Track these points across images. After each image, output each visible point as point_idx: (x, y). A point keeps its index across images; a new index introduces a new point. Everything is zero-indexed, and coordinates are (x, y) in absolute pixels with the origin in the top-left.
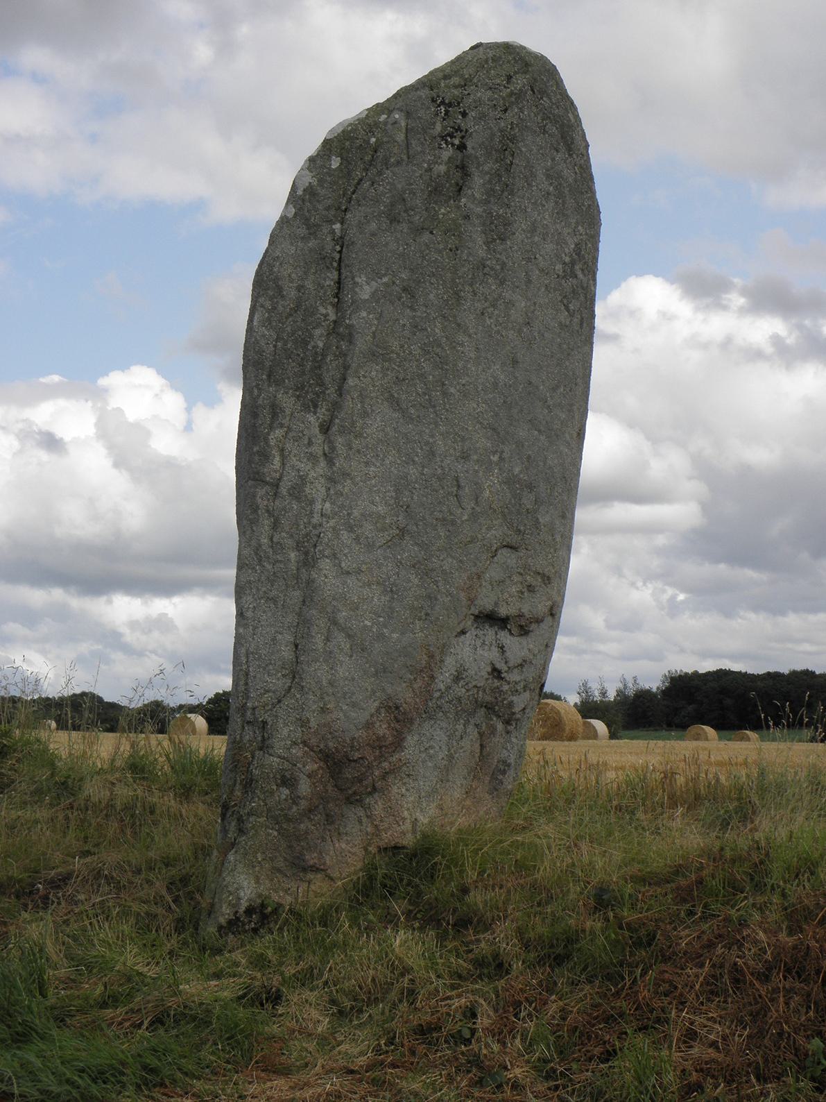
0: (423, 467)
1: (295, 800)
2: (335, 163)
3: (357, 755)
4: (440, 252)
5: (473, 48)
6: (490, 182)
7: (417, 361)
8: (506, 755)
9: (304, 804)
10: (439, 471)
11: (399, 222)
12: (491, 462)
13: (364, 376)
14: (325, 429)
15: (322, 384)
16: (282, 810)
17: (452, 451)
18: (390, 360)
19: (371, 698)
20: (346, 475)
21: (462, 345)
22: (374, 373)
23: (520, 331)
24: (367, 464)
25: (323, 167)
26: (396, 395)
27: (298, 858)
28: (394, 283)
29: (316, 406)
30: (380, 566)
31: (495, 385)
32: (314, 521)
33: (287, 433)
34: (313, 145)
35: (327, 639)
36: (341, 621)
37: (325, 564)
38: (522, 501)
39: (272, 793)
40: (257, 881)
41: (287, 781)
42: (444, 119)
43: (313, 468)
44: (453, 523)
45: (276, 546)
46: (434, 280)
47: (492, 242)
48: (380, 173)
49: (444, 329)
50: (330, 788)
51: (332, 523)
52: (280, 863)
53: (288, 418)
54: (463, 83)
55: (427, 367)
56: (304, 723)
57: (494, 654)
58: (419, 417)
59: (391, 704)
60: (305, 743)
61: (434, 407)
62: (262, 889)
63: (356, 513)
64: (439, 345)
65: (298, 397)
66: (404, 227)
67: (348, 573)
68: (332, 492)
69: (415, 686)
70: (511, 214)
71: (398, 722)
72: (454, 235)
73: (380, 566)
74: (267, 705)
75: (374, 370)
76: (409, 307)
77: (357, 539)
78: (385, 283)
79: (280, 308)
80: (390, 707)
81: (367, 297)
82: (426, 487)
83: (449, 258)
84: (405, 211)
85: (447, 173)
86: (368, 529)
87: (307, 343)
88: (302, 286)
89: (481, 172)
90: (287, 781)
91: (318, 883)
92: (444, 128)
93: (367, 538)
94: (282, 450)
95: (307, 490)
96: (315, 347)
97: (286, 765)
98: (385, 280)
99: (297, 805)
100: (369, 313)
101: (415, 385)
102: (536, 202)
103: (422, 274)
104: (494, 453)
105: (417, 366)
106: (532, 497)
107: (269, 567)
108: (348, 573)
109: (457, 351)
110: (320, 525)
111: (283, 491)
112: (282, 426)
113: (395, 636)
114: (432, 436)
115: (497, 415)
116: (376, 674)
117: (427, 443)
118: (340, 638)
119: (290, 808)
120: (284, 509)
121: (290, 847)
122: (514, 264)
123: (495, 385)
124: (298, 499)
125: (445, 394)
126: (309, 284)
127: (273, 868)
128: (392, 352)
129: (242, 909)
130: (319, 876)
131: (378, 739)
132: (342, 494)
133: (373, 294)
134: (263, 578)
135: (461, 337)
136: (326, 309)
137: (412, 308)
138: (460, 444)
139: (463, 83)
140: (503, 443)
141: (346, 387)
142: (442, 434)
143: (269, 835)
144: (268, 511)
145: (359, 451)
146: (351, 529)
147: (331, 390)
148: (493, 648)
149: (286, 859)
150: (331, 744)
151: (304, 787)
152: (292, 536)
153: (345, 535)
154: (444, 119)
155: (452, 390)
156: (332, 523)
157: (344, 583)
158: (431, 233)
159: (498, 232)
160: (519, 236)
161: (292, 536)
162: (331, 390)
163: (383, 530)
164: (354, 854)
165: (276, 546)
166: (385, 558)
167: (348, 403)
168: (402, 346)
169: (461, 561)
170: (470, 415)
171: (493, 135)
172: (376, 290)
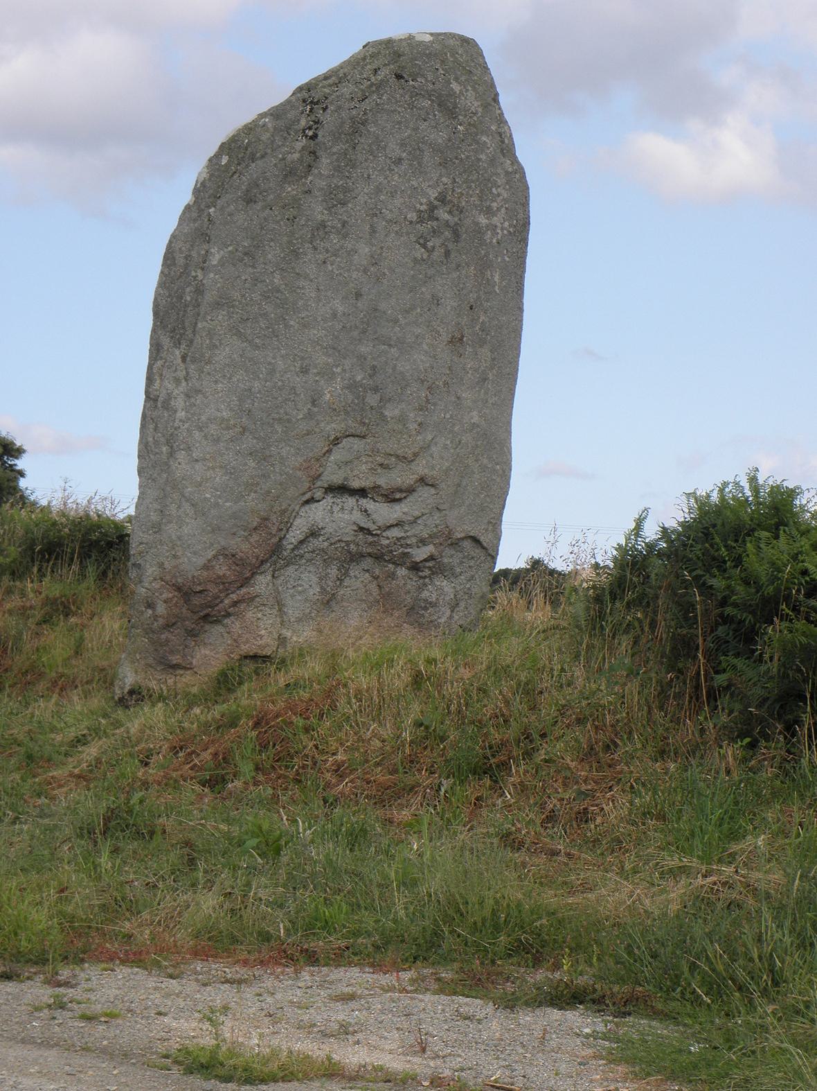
0: (266, 382)
1: (155, 618)
2: (225, 160)
3: (199, 588)
4: (278, 222)
5: (364, 47)
6: (337, 160)
7: (259, 304)
8: (428, 594)
9: (161, 621)
10: (280, 383)
11: (255, 202)
12: (334, 373)
13: (212, 320)
14: (184, 358)
15: (184, 328)
16: (148, 624)
17: (292, 368)
18: (233, 306)
19: (209, 548)
20: (198, 391)
21: (303, 288)
22: (220, 317)
23: (365, 271)
24: (216, 382)
25: (217, 164)
26: (243, 331)
27: (163, 658)
28: (237, 250)
29: (180, 344)
30: (222, 455)
31: (334, 315)
32: (176, 425)
33: (165, 363)
34: (212, 150)
35: (179, 507)
36: (187, 495)
37: (181, 456)
38: (366, 400)
39: (142, 612)
40: (136, 672)
41: (150, 605)
42: (309, 115)
43: (177, 387)
44: (289, 421)
45: (156, 443)
46: (272, 244)
47: (333, 207)
48: (247, 166)
49: (283, 278)
50: (184, 610)
51: (186, 425)
52: (151, 661)
53: (165, 353)
54: (337, 82)
55: (269, 308)
56: (161, 565)
57: (357, 516)
58: (264, 344)
59: (227, 553)
60: (162, 579)
61: (277, 336)
62: (139, 678)
63: (203, 418)
64: (278, 291)
65: (172, 337)
66: (259, 206)
67: (197, 461)
68: (187, 404)
69: (252, 540)
70: (353, 183)
71: (237, 565)
72: (293, 208)
73: (222, 455)
74: (143, 552)
75: (221, 315)
76: (250, 266)
77: (205, 437)
78: (230, 251)
79: (172, 273)
80: (226, 555)
81: (215, 263)
82: (268, 396)
83: (286, 225)
84: (260, 194)
85: (301, 160)
86: (213, 429)
87: (182, 299)
88: (190, 256)
89: (328, 154)
90: (150, 605)
91: (186, 678)
92: (308, 122)
93: (212, 435)
94: (161, 375)
95: (173, 403)
96: (185, 301)
97: (150, 594)
98: (230, 248)
99: (157, 621)
100: (215, 275)
101: (258, 322)
102: (383, 168)
103: (261, 241)
104: (337, 366)
105: (259, 308)
106: (377, 397)
107: (152, 457)
108: (197, 461)
109: (297, 293)
110: (179, 427)
111: (159, 405)
112: (161, 358)
113: (228, 504)
114: (274, 358)
115: (337, 337)
116: (213, 531)
117: (270, 363)
118: (186, 506)
119: (153, 624)
120: (159, 417)
121: (156, 650)
122: (357, 220)
123: (334, 315)
124: (167, 409)
125: (287, 326)
126: (194, 254)
127: (147, 664)
128: (234, 300)
129: (126, 691)
130: (188, 672)
131: (219, 577)
132: (195, 405)
133: (220, 260)
134: (150, 465)
135: (301, 283)
136: (196, 272)
137: (253, 267)
138: (299, 362)
139: (337, 82)
140: (345, 358)
141: (197, 329)
142: (282, 357)
143: (143, 641)
144: (152, 419)
145: (209, 374)
146: (200, 429)
147: (189, 332)
148: (354, 512)
149: (154, 659)
150: (179, 580)
151: (161, 609)
152: (164, 436)
153: (197, 434)
154: (309, 115)
155: (292, 323)
156: (186, 425)
157: (193, 468)
158: (271, 209)
159: (337, 198)
160: (362, 199)
161: (164, 436)
162: (189, 332)
163: (228, 428)
164: (218, 659)
165: (156, 443)
166: (227, 449)
167: (198, 340)
168: (243, 296)
169: (298, 449)
170: (310, 339)
171: (343, 123)
172: (223, 257)
